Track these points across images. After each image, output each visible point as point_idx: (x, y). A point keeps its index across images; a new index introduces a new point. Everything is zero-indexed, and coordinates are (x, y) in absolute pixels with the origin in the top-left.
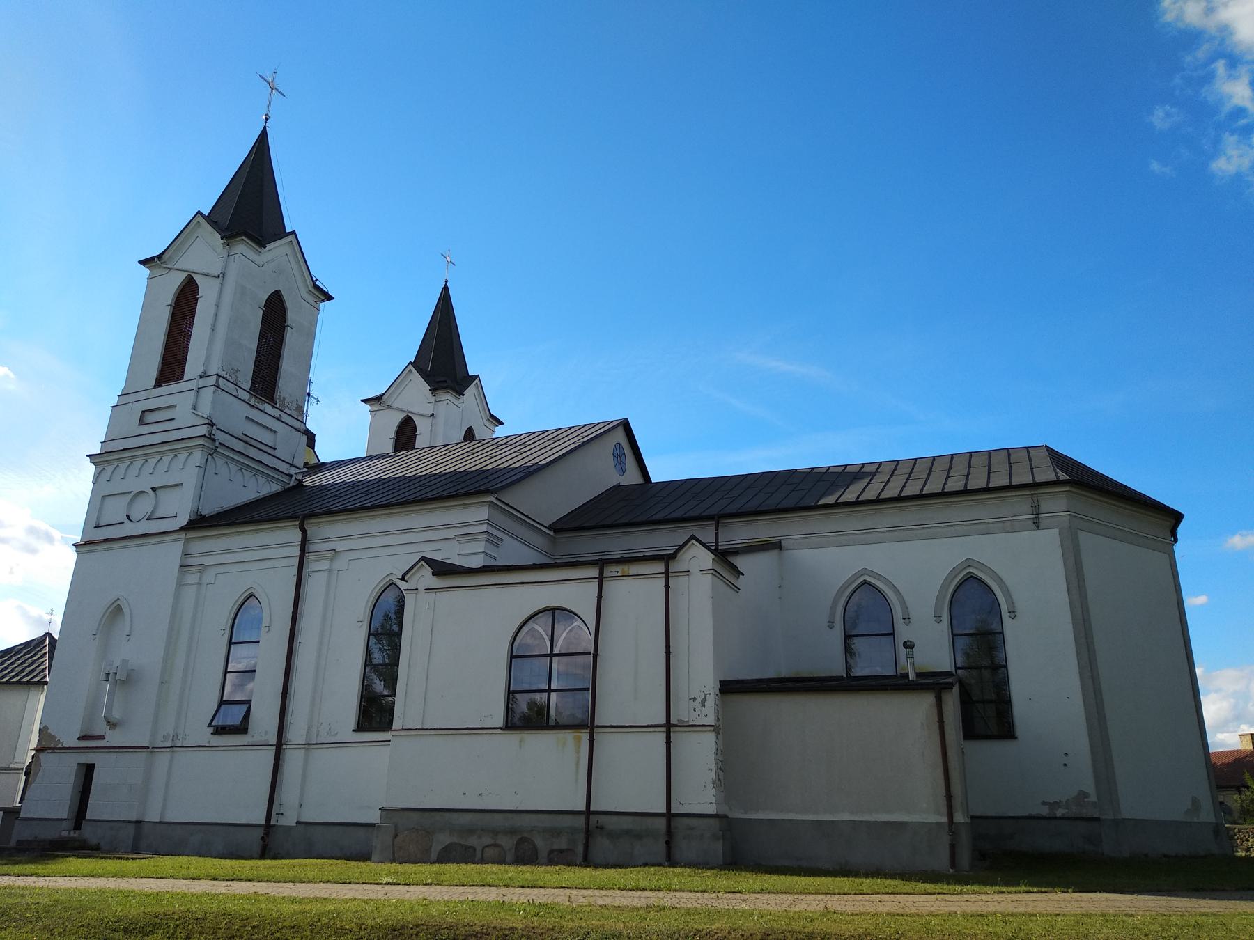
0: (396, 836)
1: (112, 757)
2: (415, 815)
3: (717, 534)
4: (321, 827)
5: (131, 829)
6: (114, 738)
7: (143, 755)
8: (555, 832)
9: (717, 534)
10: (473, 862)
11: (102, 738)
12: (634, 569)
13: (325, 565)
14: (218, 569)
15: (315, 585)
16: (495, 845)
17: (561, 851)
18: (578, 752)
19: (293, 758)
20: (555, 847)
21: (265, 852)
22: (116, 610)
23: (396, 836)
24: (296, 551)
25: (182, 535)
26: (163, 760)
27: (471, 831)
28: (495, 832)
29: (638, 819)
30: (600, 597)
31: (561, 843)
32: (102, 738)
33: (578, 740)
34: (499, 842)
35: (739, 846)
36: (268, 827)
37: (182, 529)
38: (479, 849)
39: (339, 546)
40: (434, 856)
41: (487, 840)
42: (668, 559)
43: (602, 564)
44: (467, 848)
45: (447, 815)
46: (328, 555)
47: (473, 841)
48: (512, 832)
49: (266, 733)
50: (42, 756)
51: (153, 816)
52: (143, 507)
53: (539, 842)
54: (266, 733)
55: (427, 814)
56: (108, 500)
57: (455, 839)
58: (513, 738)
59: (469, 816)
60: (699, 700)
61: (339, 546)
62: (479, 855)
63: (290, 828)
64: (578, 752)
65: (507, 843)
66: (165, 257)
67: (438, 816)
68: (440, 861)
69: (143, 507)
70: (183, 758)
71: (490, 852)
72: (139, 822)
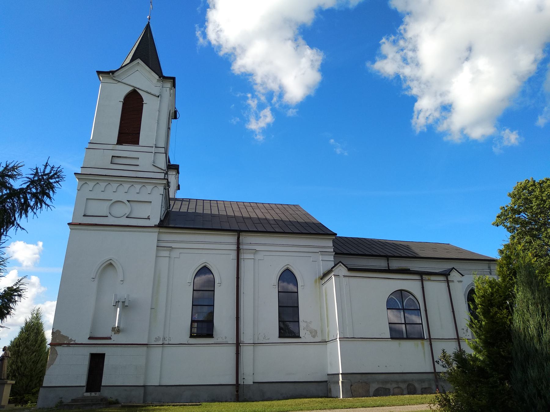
0: (351, 385)
1: (119, 349)
2: (359, 376)
3: (388, 263)
4: (268, 384)
5: (142, 391)
6: (116, 339)
7: (144, 349)
8: (422, 381)
9: (388, 263)
10: (368, 396)
11: (109, 338)
12: (433, 278)
13: (252, 256)
14: (181, 251)
15: (247, 265)
16: (398, 387)
17: (426, 388)
18: (424, 349)
19: (246, 352)
20: (424, 387)
21: (238, 399)
22: (110, 265)
23: (351, 385)
24: (235, 247)
25: (157, 230)
26: (156, 352)
27: (386, 382)
28: (397, 382)
29: (401, 375)
30: (423, 288)
31: (426, 385)
32: (109, 338)
33: (423, 344)
34: (400, 386)
35: (239, 392)
36: (237, 385)
37: (155, 226)
38: (391, 389)
39: (258, 248)
40: (371, 393)
41: (395, 385)
42: (446, 274)
43: (421, 274)
44: (386, 389)
45: (373, 375)
46: (254, 251)
47: (388, 386)
48: (404, 381)
49: (226, 338)
50: (58, 349)
51: (154, 381)
52: (124, 210)
53: (417, 385)
54: (226, 338)
55: (364, 375)
56: (90, 201)
57: (381, 386)
58: (396, 343)
59: (383, 376)
60: (465, 330)
61: (258, 248)
62: (392, 392)
63: (250, 385)
64: (424, 349)
65: (404, 386)
66: (116, 74)
67: (369, 376)
68: (375, 395)
69: (121, 210)
70: (169, 350)
71: (396, 391)
72: (144, 386)
